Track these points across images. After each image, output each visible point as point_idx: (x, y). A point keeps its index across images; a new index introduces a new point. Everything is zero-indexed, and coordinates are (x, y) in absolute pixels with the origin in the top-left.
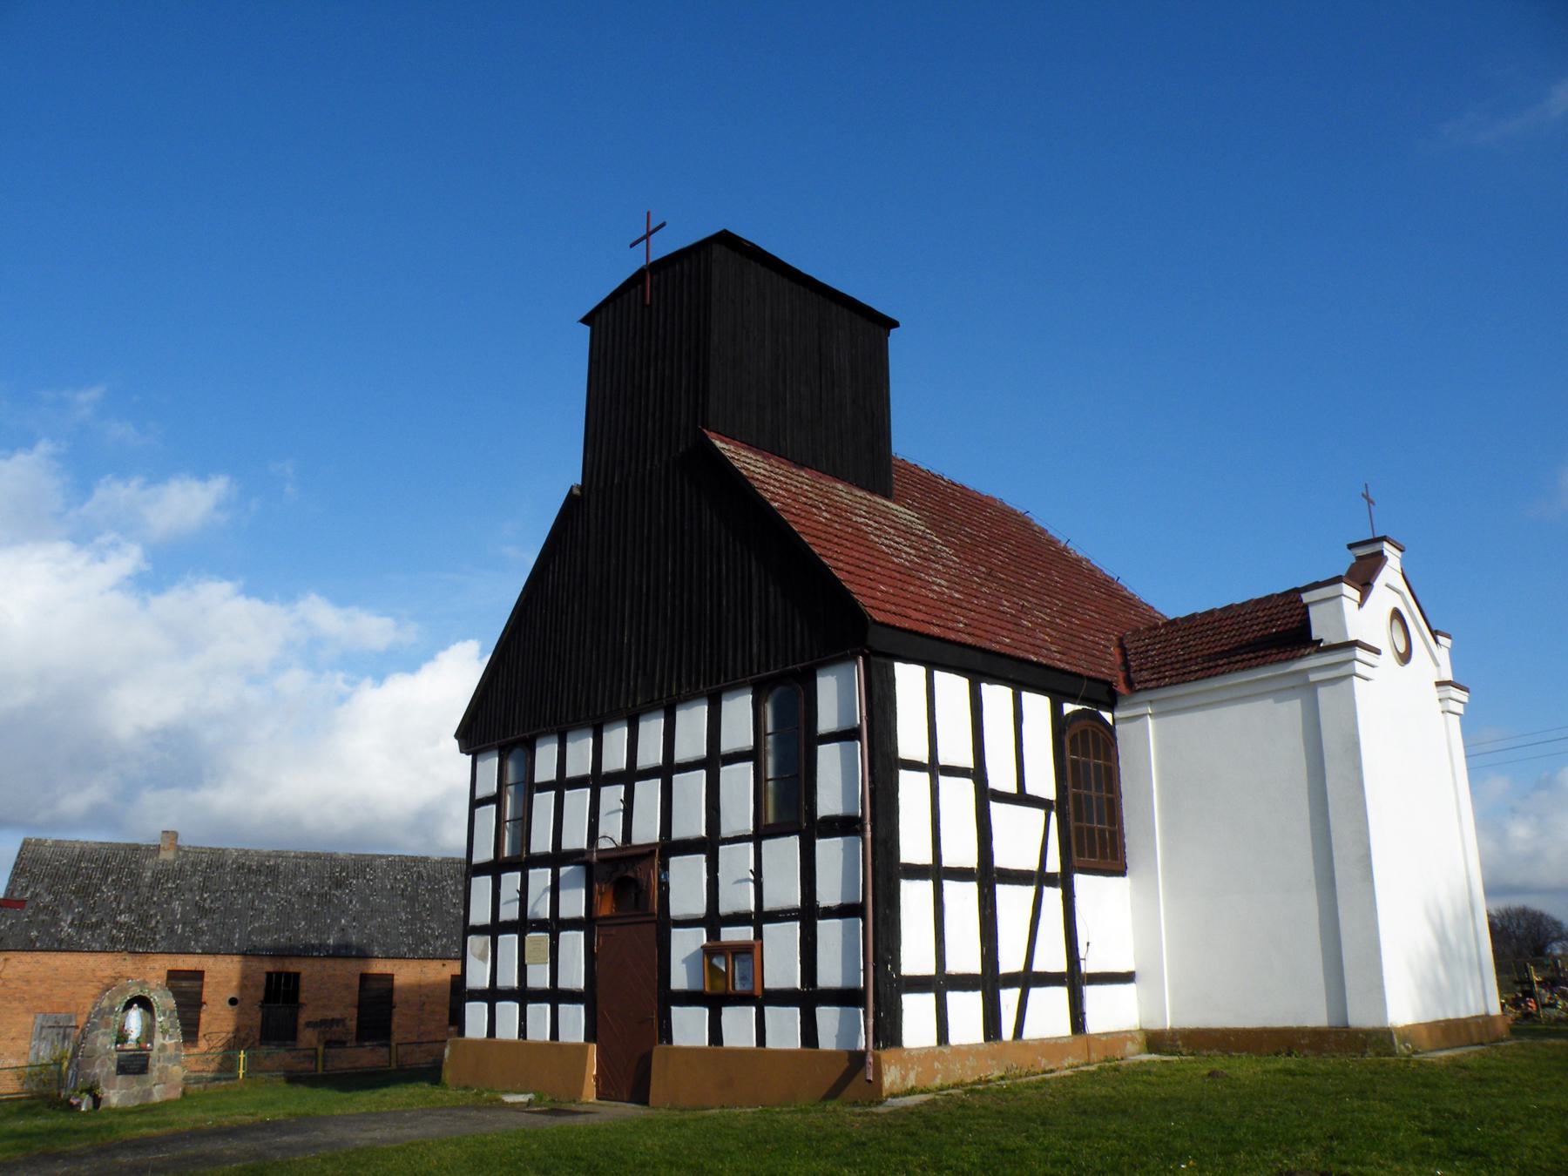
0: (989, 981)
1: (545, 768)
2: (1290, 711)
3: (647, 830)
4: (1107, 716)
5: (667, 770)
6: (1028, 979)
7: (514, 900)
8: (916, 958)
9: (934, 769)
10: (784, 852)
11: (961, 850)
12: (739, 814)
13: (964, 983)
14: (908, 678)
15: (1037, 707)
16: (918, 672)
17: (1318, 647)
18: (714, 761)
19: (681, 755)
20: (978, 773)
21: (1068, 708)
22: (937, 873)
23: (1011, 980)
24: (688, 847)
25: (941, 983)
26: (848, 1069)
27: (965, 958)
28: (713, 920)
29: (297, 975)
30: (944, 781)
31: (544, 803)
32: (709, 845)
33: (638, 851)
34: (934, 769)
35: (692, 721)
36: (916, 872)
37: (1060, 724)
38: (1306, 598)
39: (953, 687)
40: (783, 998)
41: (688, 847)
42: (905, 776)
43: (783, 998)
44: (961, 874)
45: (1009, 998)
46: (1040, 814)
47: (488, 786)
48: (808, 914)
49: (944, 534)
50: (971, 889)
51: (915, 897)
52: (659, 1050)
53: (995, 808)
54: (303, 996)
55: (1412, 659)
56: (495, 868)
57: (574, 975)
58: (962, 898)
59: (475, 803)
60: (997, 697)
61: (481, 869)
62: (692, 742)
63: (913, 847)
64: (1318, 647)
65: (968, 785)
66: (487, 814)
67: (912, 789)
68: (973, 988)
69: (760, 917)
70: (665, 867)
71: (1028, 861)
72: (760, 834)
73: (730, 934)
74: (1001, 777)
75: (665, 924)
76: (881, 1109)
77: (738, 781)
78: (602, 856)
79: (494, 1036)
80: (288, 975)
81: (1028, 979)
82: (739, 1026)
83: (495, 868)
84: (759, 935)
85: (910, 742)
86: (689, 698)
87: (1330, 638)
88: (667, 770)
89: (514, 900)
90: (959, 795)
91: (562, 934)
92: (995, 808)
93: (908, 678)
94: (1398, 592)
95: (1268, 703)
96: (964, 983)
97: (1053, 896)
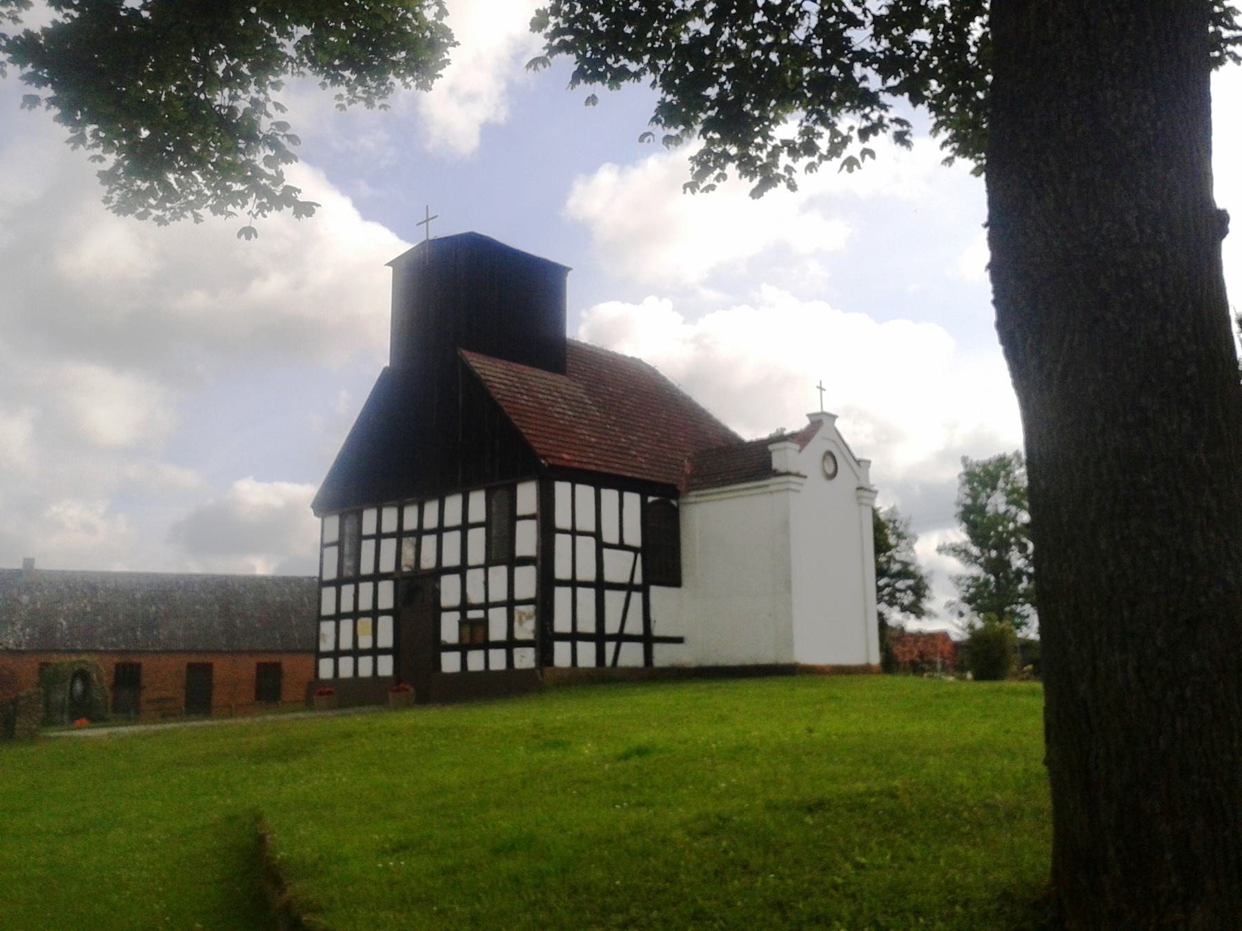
0: (599, 637)
1: (369, 526)
3: (428, 562)
4: (674, 502)
5: (440, 530)
6: (621, 638)
8: (562, 623)
9: (574, 532)
10: (499, 574)
11: (587, 571)
12: (477, 554)
13: (586, 637)
14: (562, 489)
15: (633, 501)
16: (567, 486)
17: (776, 474)
18: (465, 527)
19: (447, 523)
20: (597, 535)
21: (651, 499)
22: (573, 584)
23: (612, 638)
24: (451, 571)
25: (574, 637)
27: (587, 624)
28: (464, 606)
29: (139, 665)
30: (579, 538)
31: (368, 547)
32: (462, 569)
34: (574, 532)
35: (453, 504)
36: (563, 583)
37: (645, 506)
38: (771, 447)
39: (585, 492)
40: (498, 645)
41: (451, 571)
42: (559, 537)
43: (498, 645)
44: (586, 584)
45: (610, 647)
46: (631, 555)
47: (333, 535)
48: (511, 603)
49: (594, 396)
50: (591, 593)
51: (562, 596)
53: (606, 551)
54: (145, 680)
55: (837, 477)
56: (338, 583)
57: (386, 638)
58: (587, 597)
59: (324, 546)
60: (610, 496)
61: (329, 583)
62: (453, 515)
63: (562, 570)
64: (776, 474)
65: (591, 541)
66: (334, 551)
67: (562, 543)
69: (486, 606)
71: (624, 578)
72: (486, 567)
73: (472, 614)
74: (610, 535)
75: (437, 610)
77: (477, 538)
80: (131, 665)
81: (621, 638)
82: (476, 661)
83: (338, 583)
84: (486, 614)
85: (562, 519)
86: (451, 492)
87: (782, 469)
88: (440, 530)
90: (587, 546)
92: (606, 551)
93: (562, 489)
94: (834, 442)
96: (586, 637)
97: (637, 597)
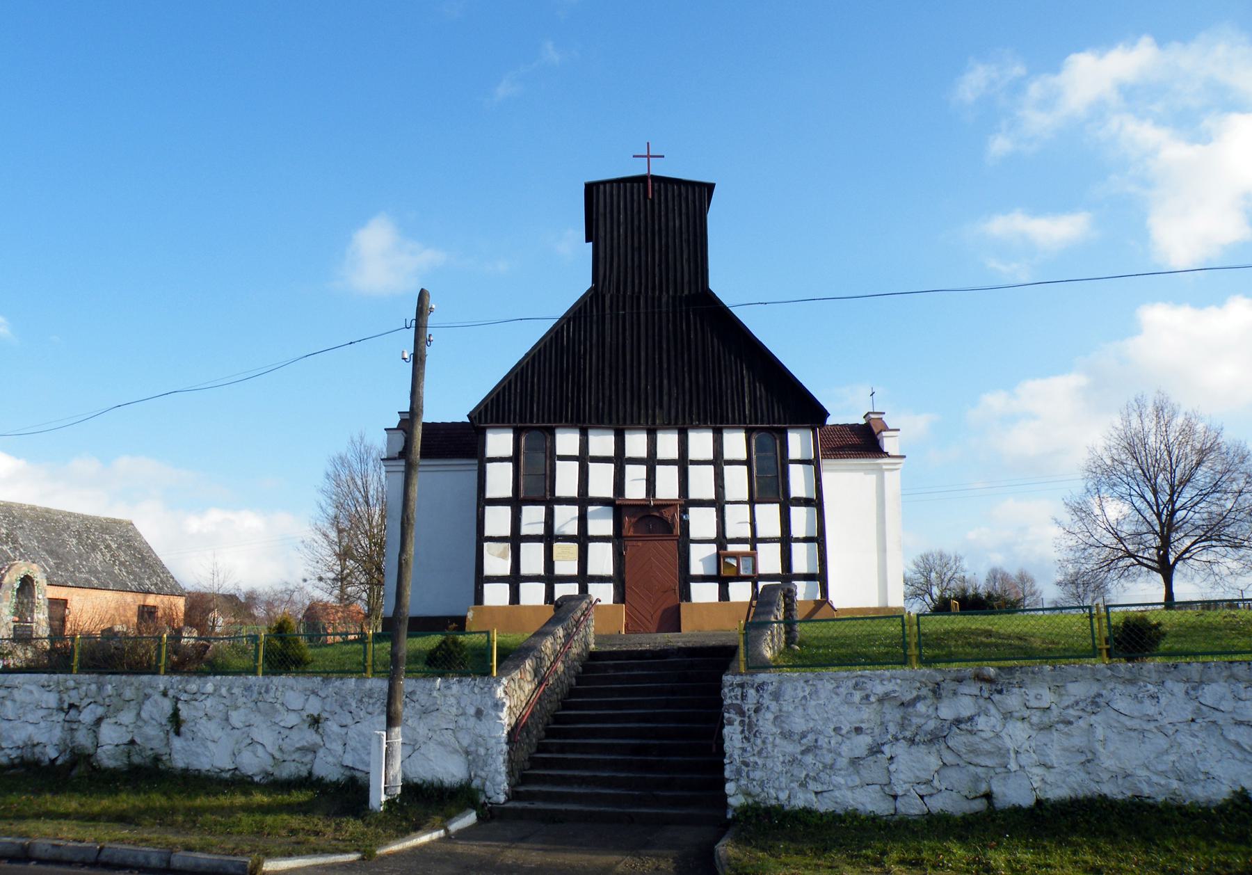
2: (871, 479)
7: (541, 523)
26: (814, 608)
33: (627, 503)
52: (684, 605)
68: (795, 575)
70: (686, 512)
76: (461, 638)
78: (656, 503)
79: (728, 599)
89: (541, 523)
91: (576, 545)
95: (861, 474)
